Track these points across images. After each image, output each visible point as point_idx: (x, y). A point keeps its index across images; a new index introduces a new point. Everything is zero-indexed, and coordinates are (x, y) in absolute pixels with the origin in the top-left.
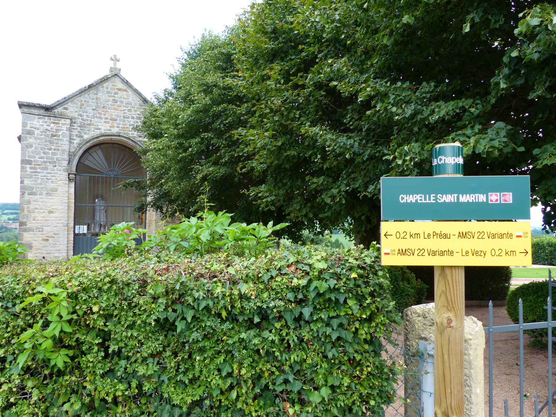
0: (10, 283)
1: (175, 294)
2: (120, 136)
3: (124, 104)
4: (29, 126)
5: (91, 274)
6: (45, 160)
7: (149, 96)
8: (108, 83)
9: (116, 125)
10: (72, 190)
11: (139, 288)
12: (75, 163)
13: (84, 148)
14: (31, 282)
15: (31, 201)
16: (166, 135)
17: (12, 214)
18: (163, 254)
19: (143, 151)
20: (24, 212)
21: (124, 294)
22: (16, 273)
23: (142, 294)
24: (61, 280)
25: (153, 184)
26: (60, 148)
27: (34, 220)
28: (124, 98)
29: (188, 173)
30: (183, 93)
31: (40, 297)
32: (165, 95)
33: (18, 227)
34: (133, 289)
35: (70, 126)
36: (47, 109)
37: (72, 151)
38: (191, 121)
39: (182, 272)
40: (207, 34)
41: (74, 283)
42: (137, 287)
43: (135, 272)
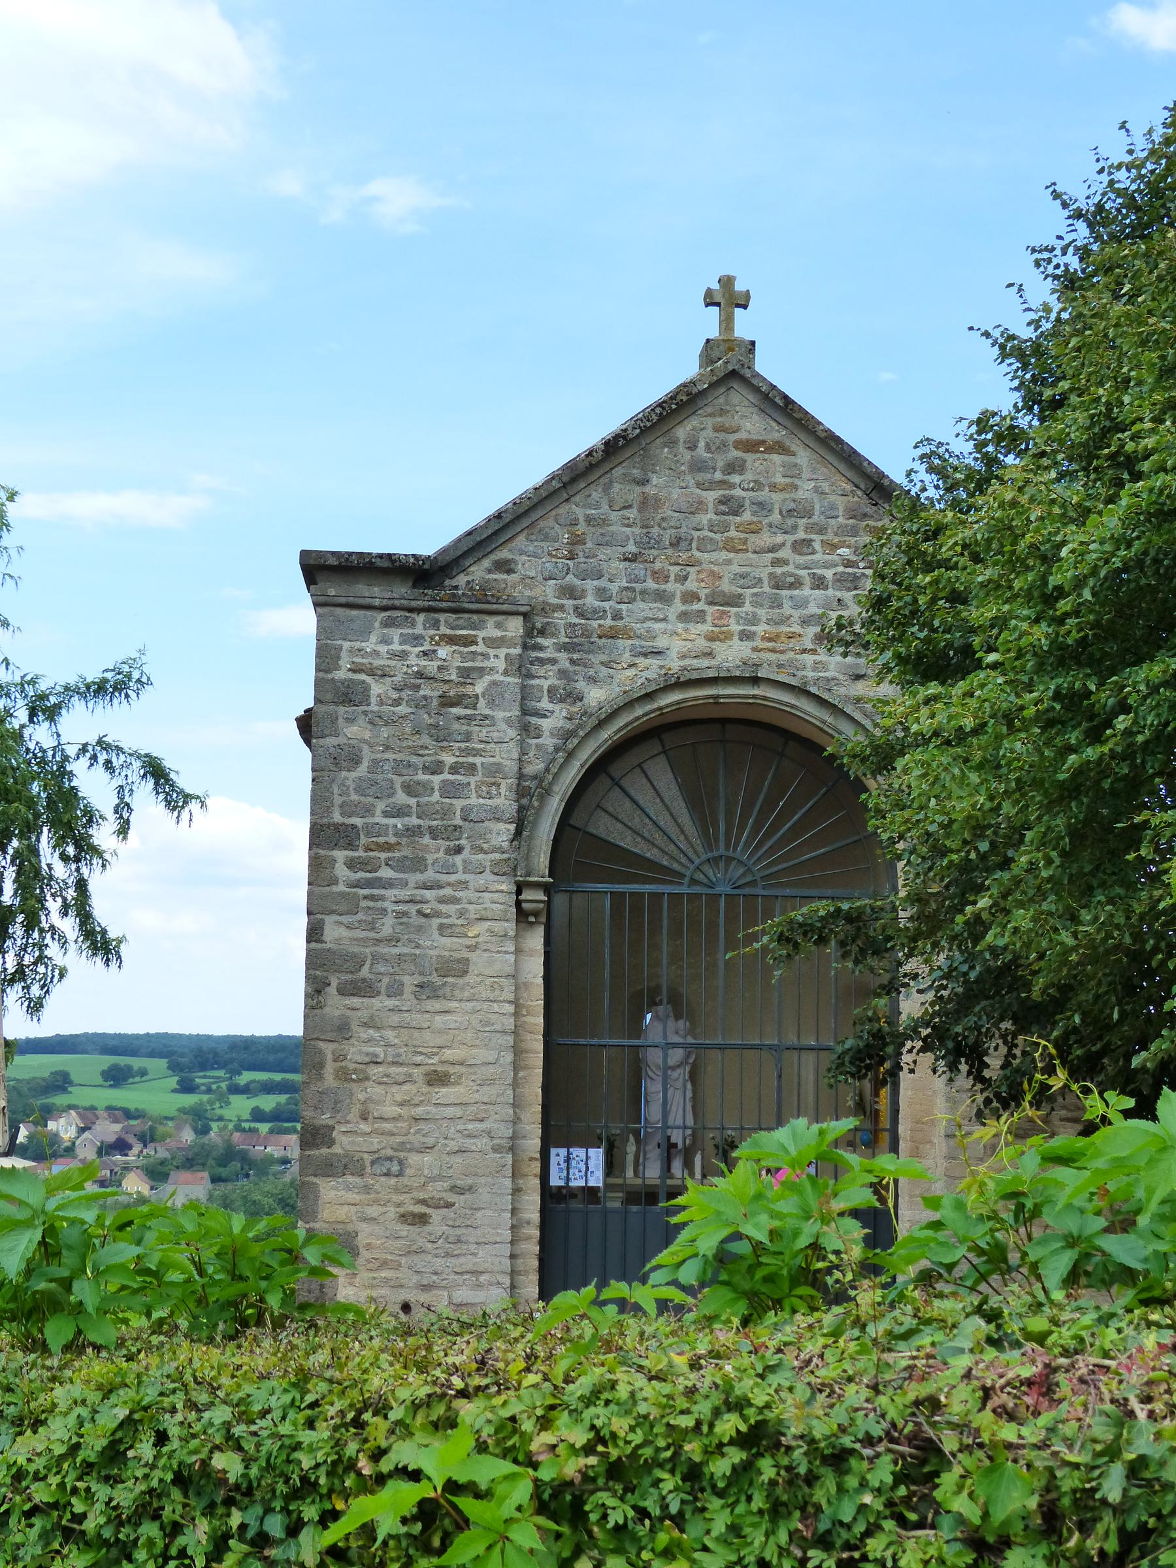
0: (277, 1414)
1: (1100, 1528)
2: (755, 681)
3: (776, 517)
4: (345, 663)
5: (651, 1390)
6: (414, 821)
7: (896, 461)
8: (694, 422)
9: (735, 628)
10: (535, 968)
11: (899, 1478)
12: (546, 829)
13: (588, 754)
14: (367, 1416)
15: (355, 1027)
16: (992, 657)
17: (269, 1088)
18: (1012, 1298)
19: (876, 749)
20: (320, 1077)
21: (818, 1508)
22: (300, 1370)
23: (913, 1517)
24: (506, 1413)
25: (930, 925)
26: (478, 760)
27: (364, 1117)
28: (773, 487)
29: (1116, 855)
30: (1074, 423)
31: (407, 1495)
32: (980, 446)
33: (295, 1153)
34: (863, 1485)
35: (525, 647)
36: (423, 576)
37: (530, 770)
38: (1126, 568)
39: (1134, 1404)
40: (1052, 224)
41: (564, 1433)
42: (883, 1473)
43: (875, 1388)
